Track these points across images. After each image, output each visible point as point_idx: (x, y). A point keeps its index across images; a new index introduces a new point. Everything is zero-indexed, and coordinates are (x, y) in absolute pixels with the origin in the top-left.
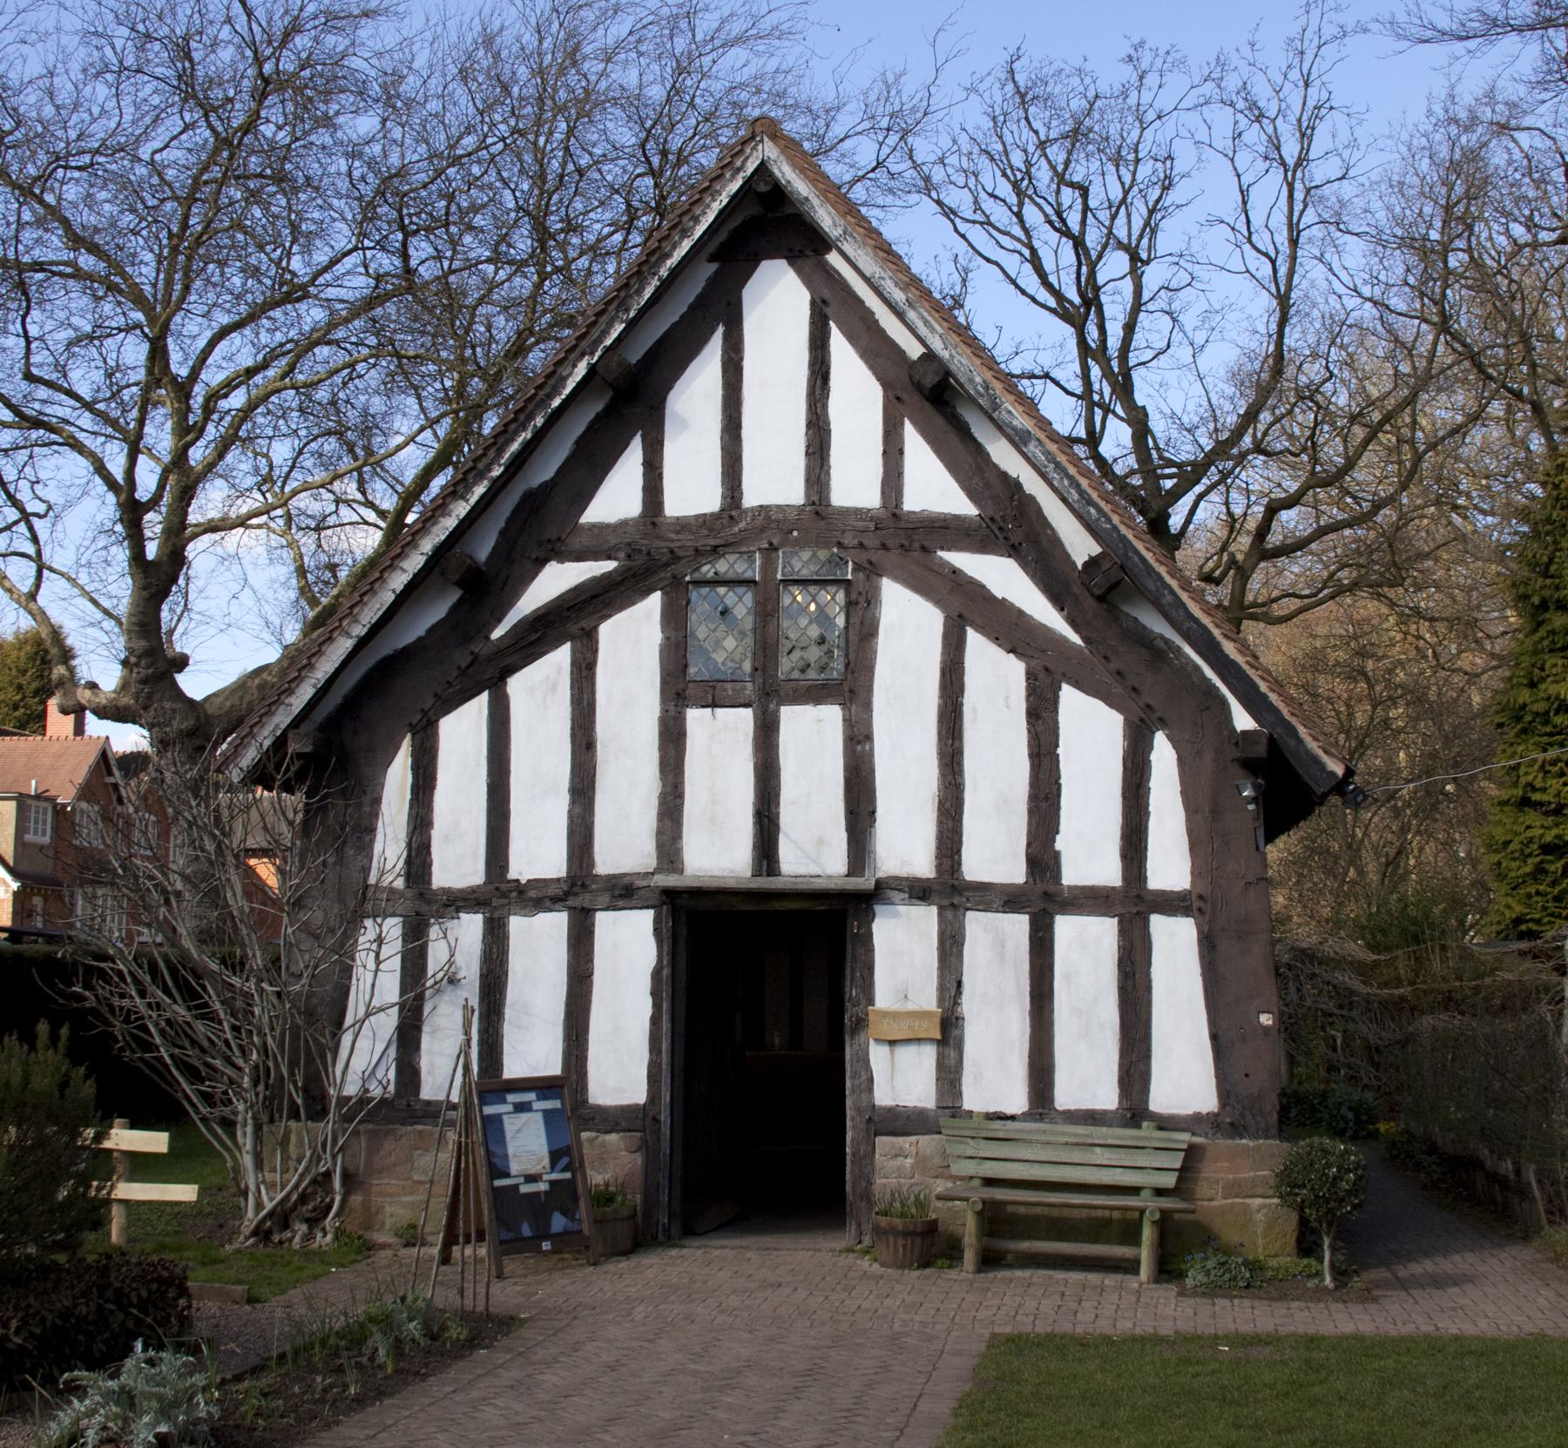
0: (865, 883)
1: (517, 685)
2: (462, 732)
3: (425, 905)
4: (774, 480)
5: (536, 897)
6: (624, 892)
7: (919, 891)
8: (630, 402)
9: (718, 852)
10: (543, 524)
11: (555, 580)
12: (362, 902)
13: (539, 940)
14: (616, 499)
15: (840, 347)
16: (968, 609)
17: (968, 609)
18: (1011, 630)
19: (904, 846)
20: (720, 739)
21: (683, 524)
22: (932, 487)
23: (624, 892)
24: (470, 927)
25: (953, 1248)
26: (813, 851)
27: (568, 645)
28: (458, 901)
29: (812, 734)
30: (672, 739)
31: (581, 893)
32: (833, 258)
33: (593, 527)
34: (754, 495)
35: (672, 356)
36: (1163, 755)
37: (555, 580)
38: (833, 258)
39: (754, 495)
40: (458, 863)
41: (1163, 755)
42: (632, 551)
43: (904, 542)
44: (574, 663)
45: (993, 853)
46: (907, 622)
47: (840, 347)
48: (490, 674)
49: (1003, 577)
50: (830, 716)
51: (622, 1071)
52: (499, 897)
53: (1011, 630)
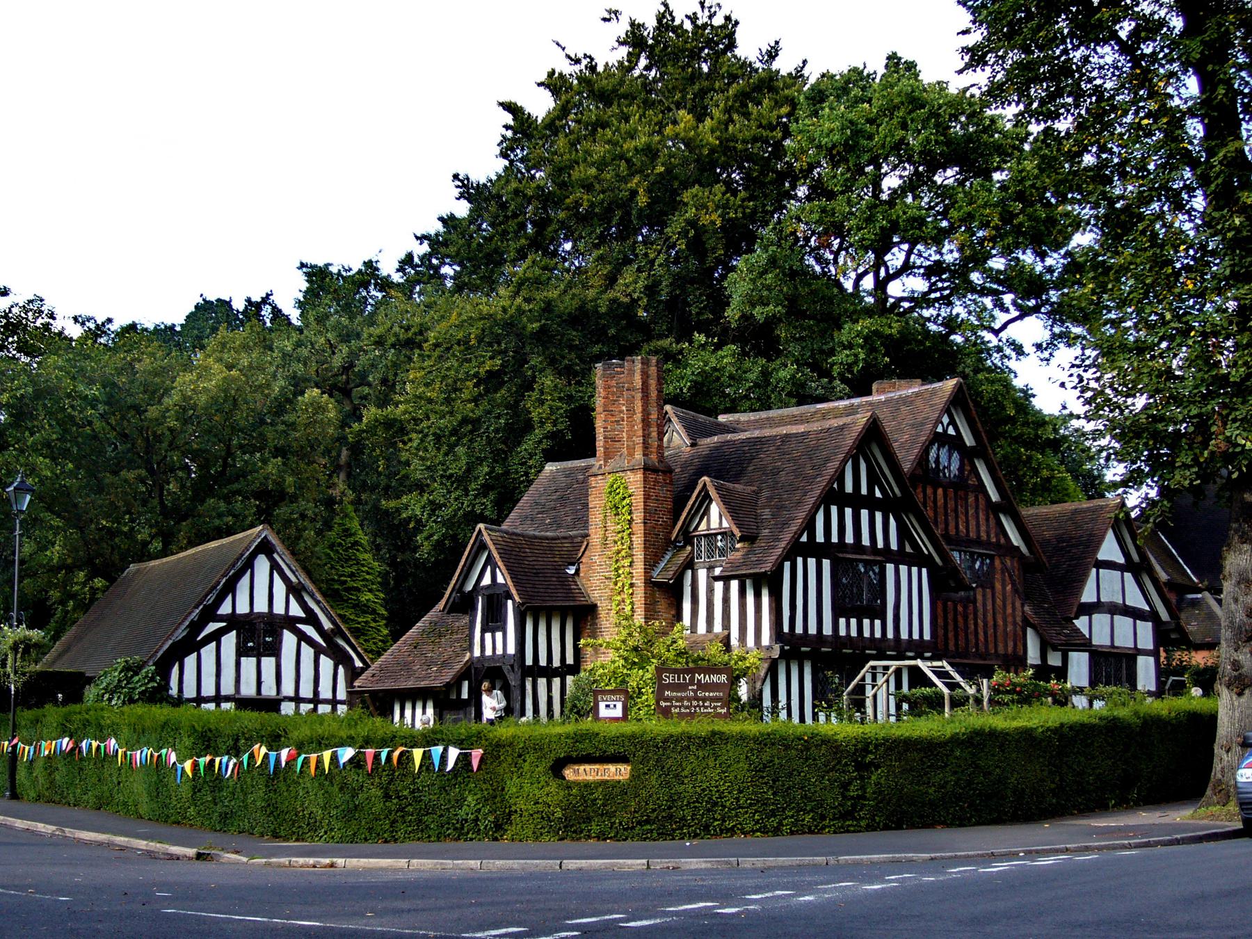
0: (280, 697)
1: (203, 651)
2: (190, 661)
4: (261, 606)
5: (208, 700)
6: (228, 699)
7: (290, 699)
8: (231, 588)
9: (248, 690)
10: (210, 614)
11: (212, 627)
14: (225, 609)
16: (302, 637)
17: (302, 637)
18: (311, 642)
19: (288, 689)
20: (249, 663)
22: (296, 610)
23: (228, 699)
29: (268, 663)
30: (238, 664)
32: (275, 556)
33: (281, 635)
34: (239, 611)
36: (341, 670)
37: (212, 627)
39: (239, 611)
41: (341, 670)
43: (290, 622)
45: (306, 692)
46: (289, 639)
49: (309, 630)
50: (273, 659)
53: (311, 642)
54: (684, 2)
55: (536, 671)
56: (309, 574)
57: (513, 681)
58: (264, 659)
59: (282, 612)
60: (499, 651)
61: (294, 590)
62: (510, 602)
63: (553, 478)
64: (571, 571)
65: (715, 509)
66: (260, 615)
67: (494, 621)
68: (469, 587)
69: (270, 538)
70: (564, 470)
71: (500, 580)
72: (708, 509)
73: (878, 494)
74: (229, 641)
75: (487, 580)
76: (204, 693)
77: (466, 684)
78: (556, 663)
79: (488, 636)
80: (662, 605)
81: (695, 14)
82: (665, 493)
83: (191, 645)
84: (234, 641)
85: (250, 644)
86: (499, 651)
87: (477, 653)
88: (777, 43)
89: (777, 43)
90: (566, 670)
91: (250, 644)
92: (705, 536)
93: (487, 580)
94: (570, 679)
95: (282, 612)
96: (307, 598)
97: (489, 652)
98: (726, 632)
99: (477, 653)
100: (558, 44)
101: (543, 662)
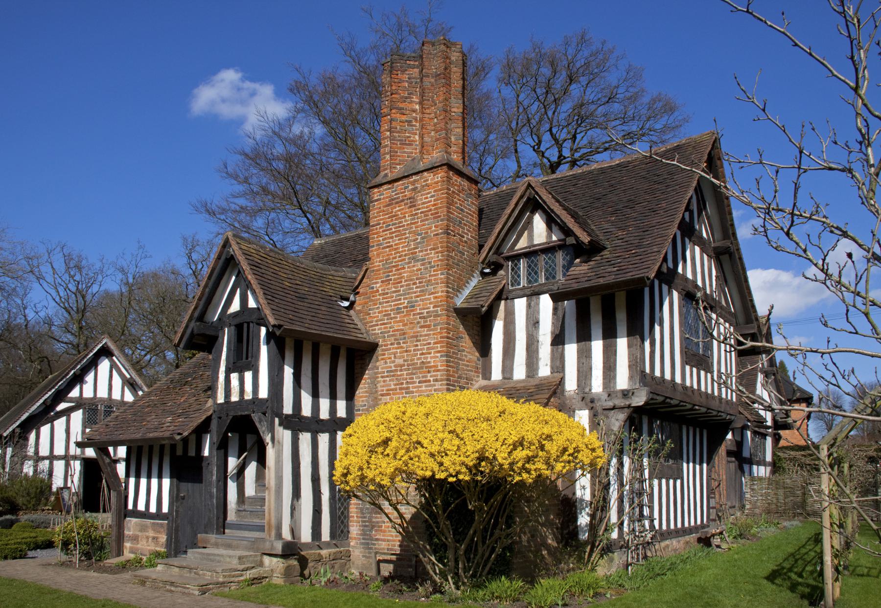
1: (56, 423)
4: (103, 393)
5: (59, 458)
8: (78, 379)
10: (60, 396)
12: (26, 458)
14: (75, 393)
15: (114, 372)
21: (86, 399)
24: (47, 462)
25: (461, 518)
28: (44, 458)
31: (67, 458)
32: (114, 358)
34: (85, 395)
35: (85, 371)
37: (62, 406)
38: (114, 358)
39: (85, 395)
40: (44, 451)
42: (77, 402)
44: (84, 419)
47: (114, 372)
48: (51, 421)
52: (52, 457)
56: (139, 372)
66: (102, 400)
67: (243, 360)
70: (333, 242)
71: (252, 304)
72: (530, 222)
75: (235, 306)
79: (234, 377)
83: (46, 415)
86: (249, 396)
93: (235, 306)
97: (235, 398)
98: (558, 376)
99: (221, 399)
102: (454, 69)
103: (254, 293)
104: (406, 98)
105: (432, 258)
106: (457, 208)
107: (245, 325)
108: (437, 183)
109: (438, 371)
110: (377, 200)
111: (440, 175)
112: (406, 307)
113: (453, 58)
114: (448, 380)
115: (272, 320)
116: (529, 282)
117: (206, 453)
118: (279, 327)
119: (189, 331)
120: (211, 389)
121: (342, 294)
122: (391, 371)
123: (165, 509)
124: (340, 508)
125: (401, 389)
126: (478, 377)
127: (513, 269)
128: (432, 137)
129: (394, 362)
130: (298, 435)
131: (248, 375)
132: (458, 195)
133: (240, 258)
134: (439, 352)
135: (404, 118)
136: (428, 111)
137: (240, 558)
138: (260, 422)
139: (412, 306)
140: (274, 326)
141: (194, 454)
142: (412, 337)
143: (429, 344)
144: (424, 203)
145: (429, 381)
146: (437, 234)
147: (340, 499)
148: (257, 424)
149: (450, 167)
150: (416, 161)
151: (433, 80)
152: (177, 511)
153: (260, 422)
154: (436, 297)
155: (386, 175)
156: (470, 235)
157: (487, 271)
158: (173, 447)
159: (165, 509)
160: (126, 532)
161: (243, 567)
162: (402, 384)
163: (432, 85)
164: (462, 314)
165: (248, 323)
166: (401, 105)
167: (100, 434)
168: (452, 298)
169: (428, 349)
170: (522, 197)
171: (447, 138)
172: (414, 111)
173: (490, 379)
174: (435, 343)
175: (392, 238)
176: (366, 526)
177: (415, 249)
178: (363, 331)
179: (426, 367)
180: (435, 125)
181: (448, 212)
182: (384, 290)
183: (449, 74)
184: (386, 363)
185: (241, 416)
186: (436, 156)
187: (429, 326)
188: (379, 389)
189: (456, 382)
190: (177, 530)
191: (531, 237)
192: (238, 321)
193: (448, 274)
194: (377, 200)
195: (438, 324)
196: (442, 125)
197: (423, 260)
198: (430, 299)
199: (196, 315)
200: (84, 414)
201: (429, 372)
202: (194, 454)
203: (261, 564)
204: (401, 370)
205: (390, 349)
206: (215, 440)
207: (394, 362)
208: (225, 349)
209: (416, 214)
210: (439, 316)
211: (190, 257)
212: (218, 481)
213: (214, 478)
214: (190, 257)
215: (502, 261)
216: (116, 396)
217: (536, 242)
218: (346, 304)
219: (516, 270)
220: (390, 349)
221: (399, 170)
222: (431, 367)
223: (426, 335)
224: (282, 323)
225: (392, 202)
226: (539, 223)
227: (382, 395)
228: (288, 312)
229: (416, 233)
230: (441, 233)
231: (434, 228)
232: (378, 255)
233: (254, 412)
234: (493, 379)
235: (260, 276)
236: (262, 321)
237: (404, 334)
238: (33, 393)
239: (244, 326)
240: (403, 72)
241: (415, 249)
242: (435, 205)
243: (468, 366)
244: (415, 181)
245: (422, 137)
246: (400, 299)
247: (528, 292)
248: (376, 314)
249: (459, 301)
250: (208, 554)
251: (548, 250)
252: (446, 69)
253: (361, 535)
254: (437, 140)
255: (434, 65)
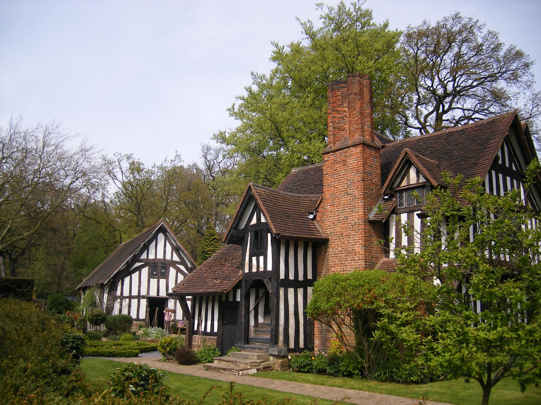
1: (133, 275)
2: (127, 280)
3: (122, 297)
4: (160, 256)
5: (134, 297)
6: (143, 297)
8: (146, 247)
9: (153, 293)
10: (136, 259)
11: (138, 264)
12: (116, 298)
13: (134, 302)
14: (144, 256)
15: (167, 242)
16: (179, 270)
20: (154, 281)
22: (176, 258)
23: (143, 297)
24: (127, 300)
26: (163, 294)
27: (171, 268)
29: (163, 282)
30: (149, 282)
31: (139, 297)
32: (167, 233)
33: (169, 269)
35: (150, 242)
37: (138, 264)
40: (126, 293)
43: (173, 264)
44: (149, 273)
46: (172, 271)
47: (167, 242)
49: (182, 267)
50: (165, 280)
51: (142, 316)
52: (130, 297)
54: (349, 0)
55: (286, 284)
57: (270, 288)
58: (161, 280)
59: (170, 259)
60: (262, 269)
61: (176, 249)
62: (269, 235)
63: (296, 174)
64: (311, 216)
65: (412, 173)
67: (259, 250)
68: (242, 226)
69: (165, 225)
70: (303, 171)
71: (263, 220)
73: (514, 168)
74: (145, 271)
75: (254, 221)
76: (133, 294)
77: (239, 292)
78: (301, 278)
79: (254, 259)
80: (376, 242)
81: (355, 3)
82: (376, 164)
83: (127, 272)
84: (147, 271)
85: (155, 273)
86: (262, 269)
87: (247, 270)
88: (387, 21)
89: (387, 21)
90: (306, 284)
91: (155, 273)
92: (406, 190)
93: (254, 221)
94: (310, 290)
95: (170, 259)
96: (181, 253)
97: (254, 270)
99: (247, 270)
100: (298, 19)
101: (291, 277)
102: (365, 89)
103: (264, 215)
104: (340, 105)
105: (356, 193)
106: (369, 165)
107: (260, 232)
108: (357, 153)
109: (360, 254)
110: (326, 161)
111: (359, 149)
112: (343, 220)
113: (365, 83)
114: (365, 259)
115: (274, 231)
116: (408, 204)
117: (238, 299)
118: (278, 234)
119: (230, 234)
120: (242, 265)
121: (309, 211)
122: (336, 254)
123: (216, 330)
124: (309, 330)
125: (341, 264)
126: (382, 256)
127: (399, 197)
128: (354, 128)
129: (337, 249)
130: (287, 289)
131: (261, 258)
132: (369, 158)
133: (257, 197)
134: (360, 244)
135: (340, 116)
136: (352, 113)
137: (258, 356)
138: (268, 283)
139: (346, 218)
140: (276, 234)
141: (232, 300)
142: (346, 236)
143: (356, 240)
144: (351, 164)
145: (356, 260)
146: (358, 181)
147: (309, 324)
148: (266, 285)
149: (364, 144)
150: (347, 139)
151: (354, 96)
152: (222, 332)
153: (268, 283)
154: (358, 215)
155: (331, 147)
156: (376, 180)
157: (386, 197)
158: (220, 297)
159: (216, 330)
160: (193, 343)
161: (259, 361)
162: (342, 261)
163: (354, 99)
164: (372, 223)
165: (261, 231)
166: (338, 109)
167: (182, 289)
168: (367, 215)
169: (355, 242)
170: (402, 159)
171: (362, 128)
172: (345, 112)
173: (389, 258)
174: (358, 239)
175: (335, 182)
176: (323, 339)
177: (347, 188)
178: (321, 232)
179: (354, 252)
180: (356, 121)
181: (364, 169)
182: (331, 210)
183: (363, 92)
184: (333, 249)
185: (258, 280)
186: (357, 138)
187: (355, 230)
188: (330, 263)
189: (370, 260)
190: (222, 342)
191: (408, 180)
192: (255, 229)
193: (364, 202)
194: (326, 161)
195: (360, 229)
196: (359, 121)
197: (351, 194)
198: (355, 216)
199: (234, 226)
200: (149, 269)
201: (356, 255)
202: (232, 300)
203: (269, 360)
204: (341, 254)
205: (335, 242)
206: (244, 292)
207: (337, 249)
208: (249, 244)
209: (347, 169)
210: (360, 225)
211: (206, 158)
212: (245, 315)
213: (243, 313)
214: (206, 158)
215: (393, 193)
216: (168, 257)
217: (411, 183)
218: (311, 216)
219: (401, 198)
220: (335, 242)
221: (338, 145)
222: (356, 252)
223: (353, 235)
224: (279, 232)
225: (335, 162)
226: (412, 173)
227: (331, 267)
228: (282, 225)
229: (347, 180)
230: (361, 180)
231: (357, 177)
232: (328, 190)
233: (265, 278)
234: (390, 257)
235: (267, 206)
236: (269, 231)
237: (342, 234)
238: (112, 255)
239: (259, 232)
240: (338, 90)
241: (347, 188)
242: (356, 165)
243: (376, 251)
244: (346, 152)
245: (349, 127)
246: (340, 215)
247: (407, 210)
248: (327, 223)
249: (371, 216)
250: (242, 355)
251: (419, 187)
252: (360, 90)
253: (320, 344)
254: (357, 129)
255: (356, 89)
